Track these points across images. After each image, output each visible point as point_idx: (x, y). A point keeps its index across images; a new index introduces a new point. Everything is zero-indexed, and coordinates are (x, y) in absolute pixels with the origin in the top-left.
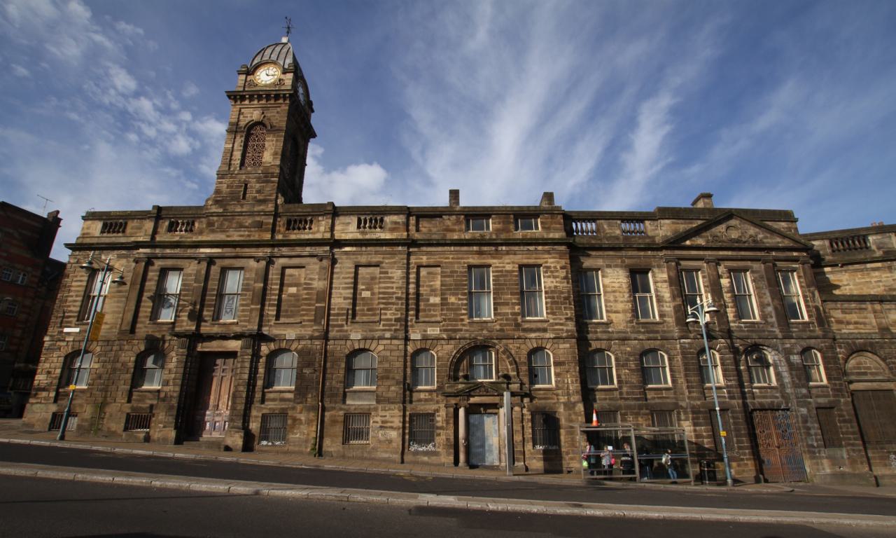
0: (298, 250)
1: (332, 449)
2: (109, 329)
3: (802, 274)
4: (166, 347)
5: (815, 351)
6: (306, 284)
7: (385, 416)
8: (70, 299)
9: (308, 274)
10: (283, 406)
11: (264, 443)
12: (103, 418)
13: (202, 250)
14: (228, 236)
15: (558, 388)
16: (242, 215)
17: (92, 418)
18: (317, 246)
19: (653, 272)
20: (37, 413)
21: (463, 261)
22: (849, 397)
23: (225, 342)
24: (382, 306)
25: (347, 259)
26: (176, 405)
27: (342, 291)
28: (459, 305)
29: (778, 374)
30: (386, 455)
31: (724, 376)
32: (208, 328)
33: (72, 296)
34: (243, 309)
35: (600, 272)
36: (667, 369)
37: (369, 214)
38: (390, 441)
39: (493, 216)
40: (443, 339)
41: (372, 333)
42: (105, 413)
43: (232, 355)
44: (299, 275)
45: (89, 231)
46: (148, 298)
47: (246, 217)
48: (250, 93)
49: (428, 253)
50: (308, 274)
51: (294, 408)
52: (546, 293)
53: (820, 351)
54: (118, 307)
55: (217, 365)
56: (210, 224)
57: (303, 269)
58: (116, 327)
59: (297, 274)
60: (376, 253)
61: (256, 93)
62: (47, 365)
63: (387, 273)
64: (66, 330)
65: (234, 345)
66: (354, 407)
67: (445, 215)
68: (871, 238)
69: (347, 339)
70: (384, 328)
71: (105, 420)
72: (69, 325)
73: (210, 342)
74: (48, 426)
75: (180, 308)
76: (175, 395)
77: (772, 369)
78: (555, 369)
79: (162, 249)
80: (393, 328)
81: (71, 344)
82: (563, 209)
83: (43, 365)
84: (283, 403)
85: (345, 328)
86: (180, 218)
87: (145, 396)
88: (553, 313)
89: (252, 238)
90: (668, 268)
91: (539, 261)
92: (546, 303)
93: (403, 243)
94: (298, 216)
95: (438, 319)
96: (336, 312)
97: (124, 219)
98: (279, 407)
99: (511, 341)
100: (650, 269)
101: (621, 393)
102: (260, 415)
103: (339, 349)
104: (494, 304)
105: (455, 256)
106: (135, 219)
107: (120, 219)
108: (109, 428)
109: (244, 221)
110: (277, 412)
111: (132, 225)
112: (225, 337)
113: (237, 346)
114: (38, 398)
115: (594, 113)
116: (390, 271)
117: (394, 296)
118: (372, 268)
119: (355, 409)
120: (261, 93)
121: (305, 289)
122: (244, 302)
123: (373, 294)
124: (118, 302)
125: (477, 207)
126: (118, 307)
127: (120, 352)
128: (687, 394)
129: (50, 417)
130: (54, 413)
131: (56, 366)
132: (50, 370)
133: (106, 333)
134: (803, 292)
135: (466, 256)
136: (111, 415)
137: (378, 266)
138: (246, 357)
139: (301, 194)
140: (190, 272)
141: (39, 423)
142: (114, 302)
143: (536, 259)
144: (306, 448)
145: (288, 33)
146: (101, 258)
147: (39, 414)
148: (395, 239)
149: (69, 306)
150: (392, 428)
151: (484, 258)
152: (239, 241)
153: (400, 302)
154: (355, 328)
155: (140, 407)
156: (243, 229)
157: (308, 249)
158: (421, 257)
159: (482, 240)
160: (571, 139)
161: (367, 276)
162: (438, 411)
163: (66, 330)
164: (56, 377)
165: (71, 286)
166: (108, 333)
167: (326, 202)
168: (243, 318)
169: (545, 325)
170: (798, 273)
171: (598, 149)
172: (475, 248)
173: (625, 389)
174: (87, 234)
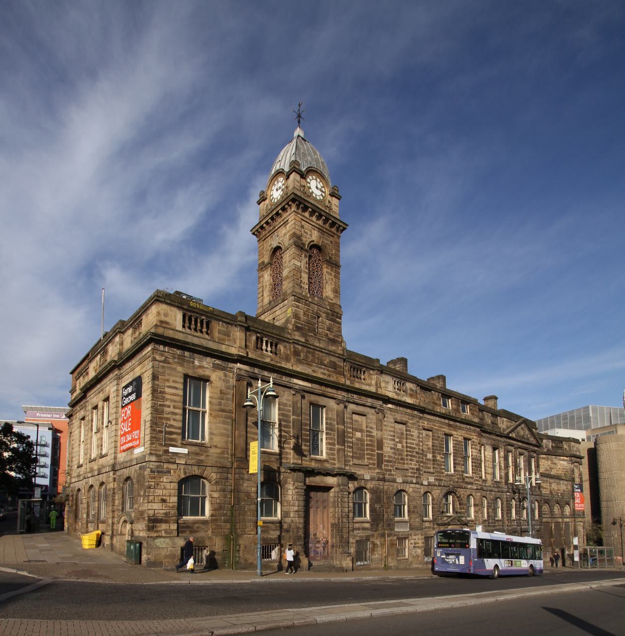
0: (364, 400)
1: (391, 565)
2: (220, 454)
4: (281, 479)
5: (366, 491)
6: (367, 431)
7: (415, 539)
8: (166, 409)
10: (367, 534)
11: (359, 563)
12: (239, 551)
13: (296, 381)
14: (314, 371)
15: (476, 520)
16: (321, 352)
17: (224, 550)
18: (376, 399)
19: (499, 450)
20: (163, 548)
21: (442, 429)
23: (325, 477)
24: (409, 458)
26: (303, 535)
28: (441, 462)
29: (527, 513)
30: (416, 566)
31: (516, 514)
33: (169, 407)
34: (330, 448)
35: (324, 409)
38: (418, 556)
39: (453, 398)
40: (436, 486)
42: (240, 545)
43: (327, 489)
45: (167, 319)
46: (253, 423)
48: (314, 208)
49: (428, 420)
51: (373, 535)
54: (225, 429)
56: (296, 353)
57: (365, 417)
59: (360, 420)
62: (159, 492)
64: (172, 449)
65: (331, 481)
66: (400, 534)
67: (433, 391)
69: (394, 481)
70: (411, 475)
71: (241, 552)
73: (315, 477)
77: (525, 510)
79: (260, 370)
81: (182, 467)
84: (364, 531)
85: (393, 473)
87: (268, 527)
88: (475, 473)
89: (332, 379)
93: (420, 409)
94: (358, 365)
95: (432, 470)
96: (387, 459)
97: (207, 317)
98: (365, 535)
100: (498, 448)
101: (489, 523)
102: (355, 541)
104: (454, 463)
105: (439, 425)
106: (220, 320)
107: (204, 315)
108: (246, 560)
109: (324, 358)
110: (364, 538)
112: (327, 474)
114: (157, 531)
115: (207, 159)
117: (415, 450)
118: (401, 425)
120: (323, 213)
121: (367, 436)
122: (330, 441)
123: (403, 447)
124: (224, 423)
125: (357, 355)
126: (225, 429)
127: (241, 481)
128: (507, 523)
131: (170, 494)
132: (164, 498)
133: (218, 458)
135: (443, 426)
136: (245, 547)
137: (404, 424)
140: (285, 401)
141: (168, 560)
142: (220, 423)
143: (470, 435)
144: (382, 565)
145: (299, 122)
147: (165, 550)
150: (418, 547)
151: (450, 430)
152: (322, 379)
154: (398, 474)
157: (369, 400)
158: (424, 422)
160: (173, 180)
163: (172, 449)
165: (164, 392)
167: (375, 358)
169: (472, 480)
170: (535, 459)
171: (201, 209)
172: (447, 421)
173: (490, 521)
174: (166, 323)
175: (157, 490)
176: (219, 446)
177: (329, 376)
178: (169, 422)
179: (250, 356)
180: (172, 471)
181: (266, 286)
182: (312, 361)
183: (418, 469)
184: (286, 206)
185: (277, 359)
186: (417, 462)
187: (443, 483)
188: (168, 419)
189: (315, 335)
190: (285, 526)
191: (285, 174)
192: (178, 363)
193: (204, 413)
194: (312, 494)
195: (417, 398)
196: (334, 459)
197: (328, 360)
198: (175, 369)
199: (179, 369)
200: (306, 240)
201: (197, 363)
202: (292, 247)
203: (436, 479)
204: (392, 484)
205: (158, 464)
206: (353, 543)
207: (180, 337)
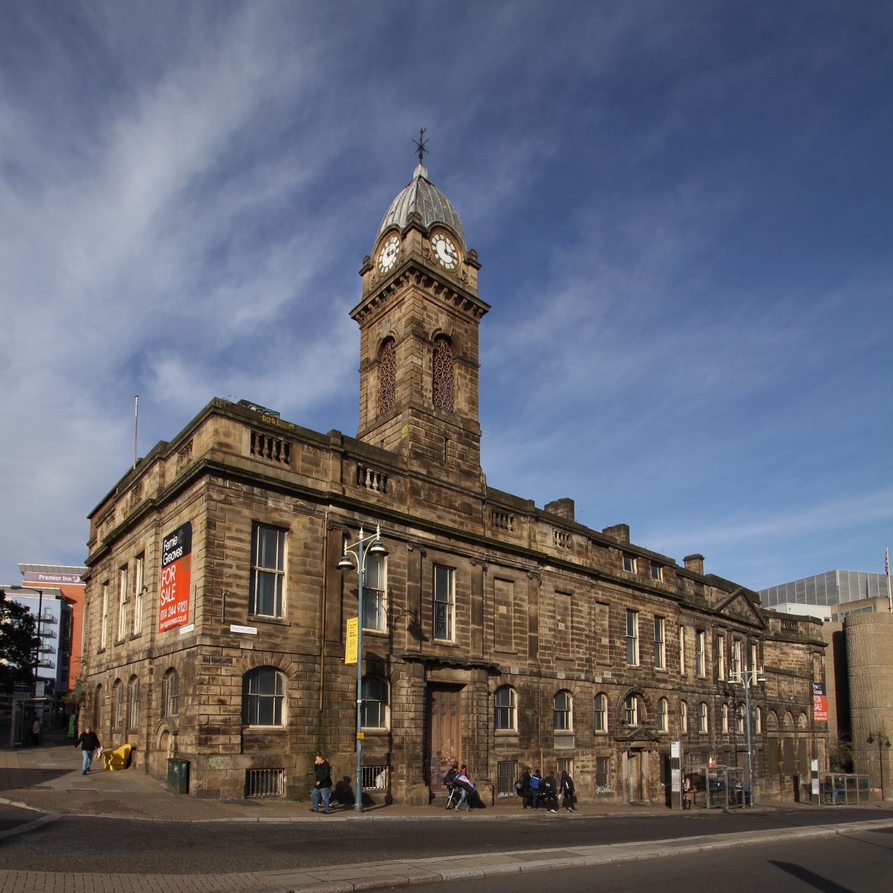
3: (758, 648)
5: (512, 690)
8: (226, 570)
9: (518, 593)
11: (502, 795)
14: (439, 517)
15: (671, 734)
16: (450, 489)
17: (307, 775)
19: (705, 634)
20: (220, 770)
22: (394, 754)
23: (454, 670)
25: (549, 580)
27: (547, 620)
29: (745, 725)
31: (729, 725)
32: (429, 650)
33: (230, 566)
34: (462, 628)
36: (571, 714)
37: (561, 528)
38: (587, 785)
39: (640, 558)
41: (572, 673)
43: (457, 687)
44: (508, 591)
47: (454, 493)
48: (442, 282)
49: (603, 589)
50: (518, 593)
52: (667, 645)
53: (669, 703)
55: (434, 700)
58: (314, 632)
59: (505, 588)
60: (571, 579)
61: (449, 286)
63: (577, 605)
65: (463, 675)
66: (562, 753)
67: (611, 547)
68: (771, 621)
69: (553, 677)
70: (579, 668)
72: (237, 619)
73: (439, 670)
74: (242, 791)
75: (395, 616)
76: (419, 740)
77: (742, 720)
78: (669, 717)
80: (585, 668)
81: (249, 654)
82: (676, 563)
83: (208, 690)
84: (510, 749)
85: (552, 664)
86: (372, 465)
87: (372, 742)
88: (671, 666)
89: (465, 529)
90: (713, 632)
91: (665, 614)
92: (667, 656)
95: (608, 662)
97: (287, 437)
98: (510, 753)
99: (650, 690)
100: (703, 631)
101: (690, 738)
103: (551, 687)
104: (640, 652)
109: (454, 499)
110: (509, 759)
111: (301, 452)
112: (458, 666)
113: (467, 677)
114: (212, 746)
115: (316, 200)
116: (580, 603)
119: (564, 754)
121: (516, 611)
127: (333, 675)
129: (244, 776)
130: (248, 772)
132: (222, 698)
134: (757, 663)
138: (483, 694)
139: (802, 616)
141: (227, 788)
145: (421, 157)
146: (266, 503)
147: (224, 773)
148: (582, 567)
149: (229, 585)
153: (588, 640)
155: (375, 757)
156: (452, 511)
157: (519, 559)
159: (633, 583)
160: (266, 231)
161: (562, 605)
162: (612, 754)
164: (236, 711)
165: (223, 546)
166: (303, 641)
167: (527, 499)
168: (463, 641)
169: (666, 677)
172: (630, 591)
175: (212, 687)
176: (302, 624)
177: (461, 524)
178: (230, 589)
179: (348, 494)
180: (234, 660)
181: (371, 393)
182: (438, 503)
183: (588, 660)
184: (401, 279)
185: (387, 499)
186: (587, 649)
187: (623, 681)
188: (229, 585)
189: (442, 464)
190: (396, 741)
191: (401, 232)
192: (244, 504)
193: (281, 576)
194: (436, 695)
195: (587, 557)
196: (467, 645)
197: (460, 502)
198: (239, 513)
199: (246, 512)
200: (430, 328)
201: (271, 504)
202: (409, 338)
203: (614, 675)
204: (550, 681)
205: (215, 649)
206: (493, 766)
207: (248, 466)
